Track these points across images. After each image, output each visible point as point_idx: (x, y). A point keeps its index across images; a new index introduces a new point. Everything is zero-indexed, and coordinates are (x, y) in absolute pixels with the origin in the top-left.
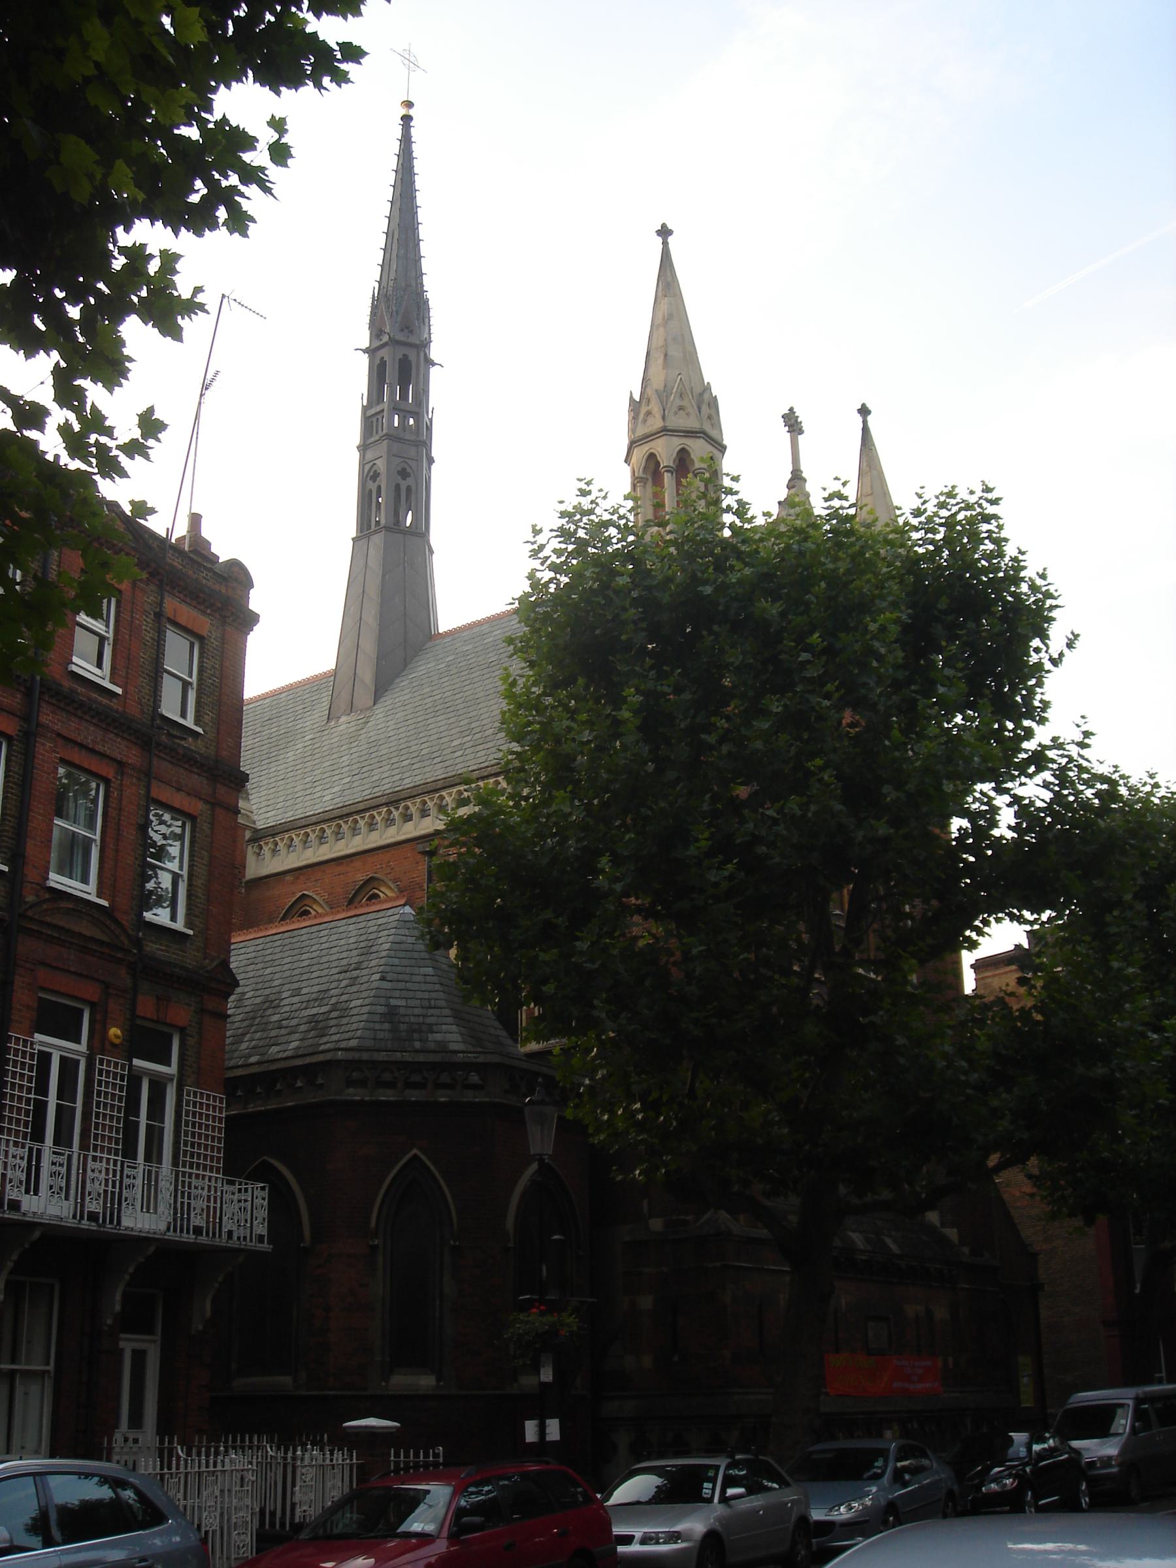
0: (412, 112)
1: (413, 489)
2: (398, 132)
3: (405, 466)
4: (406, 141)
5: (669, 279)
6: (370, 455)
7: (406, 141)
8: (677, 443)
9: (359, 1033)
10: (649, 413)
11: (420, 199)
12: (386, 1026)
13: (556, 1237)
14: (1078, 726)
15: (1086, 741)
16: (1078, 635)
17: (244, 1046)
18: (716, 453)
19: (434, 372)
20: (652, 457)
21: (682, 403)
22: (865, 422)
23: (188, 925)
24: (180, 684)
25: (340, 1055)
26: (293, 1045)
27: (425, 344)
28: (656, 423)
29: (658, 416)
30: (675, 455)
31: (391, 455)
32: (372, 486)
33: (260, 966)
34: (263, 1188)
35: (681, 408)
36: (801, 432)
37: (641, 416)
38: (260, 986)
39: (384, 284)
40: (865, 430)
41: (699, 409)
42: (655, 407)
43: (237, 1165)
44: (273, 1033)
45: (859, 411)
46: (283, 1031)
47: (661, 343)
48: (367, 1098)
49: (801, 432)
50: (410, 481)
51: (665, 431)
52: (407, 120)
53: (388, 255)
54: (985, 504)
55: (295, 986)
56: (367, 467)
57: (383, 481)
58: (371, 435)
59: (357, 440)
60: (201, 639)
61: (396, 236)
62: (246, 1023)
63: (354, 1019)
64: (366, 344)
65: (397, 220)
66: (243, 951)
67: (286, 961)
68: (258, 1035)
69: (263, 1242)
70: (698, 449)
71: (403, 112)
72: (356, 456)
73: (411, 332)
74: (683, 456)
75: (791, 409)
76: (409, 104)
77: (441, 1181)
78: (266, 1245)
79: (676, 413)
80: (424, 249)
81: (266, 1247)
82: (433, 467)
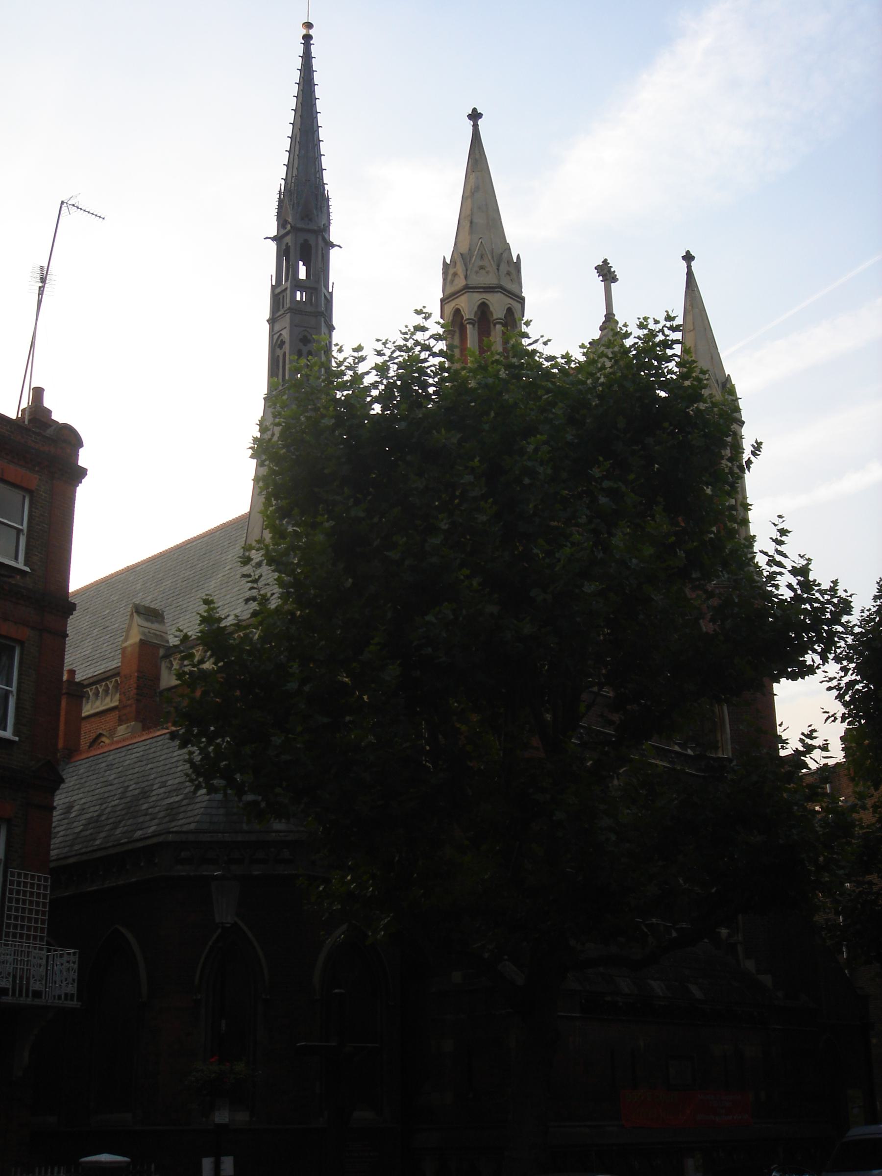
0: (311, 32)
2: (300, 49)
4: (307, 57)
5: (477, 156)
6: (277, 327)
7: (307, 57)
8: (477, 298)
9: (197, 818)
10: (455, 274)
11: (320, 106)
12: (222, 811)
13: (336, 991)
14: (775, 525)
15: (784, 538)
16: (761, 443)
17: (118, 831)
18: (516, 306)
19: (333, 253)
20: (457, 312)
21: (481, 263)
22: (689, 267)
23: (16, 732)
24: (14, 532)
25: (170, 837)
26: (153, 828)
27: (325, 229)
28: (460, 282)
29: (462, 277)
30: (476, 308)
31: (293, 325)
32: (279, 352)
33: (144, 763)
34: (74, 953)
35: (482, 268)
36: (614, 279)
37: (449, 277)
38: (140, 780)
39: (289, 181)
40: (690, 275)
41: (498, 266)
42: (460, 269)
43: (59, 933)
44: (141, 820)
45: (684, 258)
46: (148, 818)
47: (469, 212)
48: (192, 874)
49: (614, 279)
51: (467, 289)
52: (307, 38)
53: (292, 156)
54: (667, 332)
55: (164, 779)
56: (276, 337)
57: (287, 347)
58: (279, 310)
59: (267, 314)
60: (30, 492)
61: (298, 139)
62: (123, 812)
63: (198, 806)
64: (274, 232)
65: (299, 126)
66: (135, 750)
67: (163, 757)
68: (130, 822)
69: (72, 1000)
70: (498, 304)
71: (304, 32)
72: (267, 327)
73: (310, 220)
74: (483, 310)
75: (605, 262)
76: (308, 25)
77: (210, 943)
78: (75, 1002)
79: (477, 272)
80: (324, 148)
81: (75, 1003)
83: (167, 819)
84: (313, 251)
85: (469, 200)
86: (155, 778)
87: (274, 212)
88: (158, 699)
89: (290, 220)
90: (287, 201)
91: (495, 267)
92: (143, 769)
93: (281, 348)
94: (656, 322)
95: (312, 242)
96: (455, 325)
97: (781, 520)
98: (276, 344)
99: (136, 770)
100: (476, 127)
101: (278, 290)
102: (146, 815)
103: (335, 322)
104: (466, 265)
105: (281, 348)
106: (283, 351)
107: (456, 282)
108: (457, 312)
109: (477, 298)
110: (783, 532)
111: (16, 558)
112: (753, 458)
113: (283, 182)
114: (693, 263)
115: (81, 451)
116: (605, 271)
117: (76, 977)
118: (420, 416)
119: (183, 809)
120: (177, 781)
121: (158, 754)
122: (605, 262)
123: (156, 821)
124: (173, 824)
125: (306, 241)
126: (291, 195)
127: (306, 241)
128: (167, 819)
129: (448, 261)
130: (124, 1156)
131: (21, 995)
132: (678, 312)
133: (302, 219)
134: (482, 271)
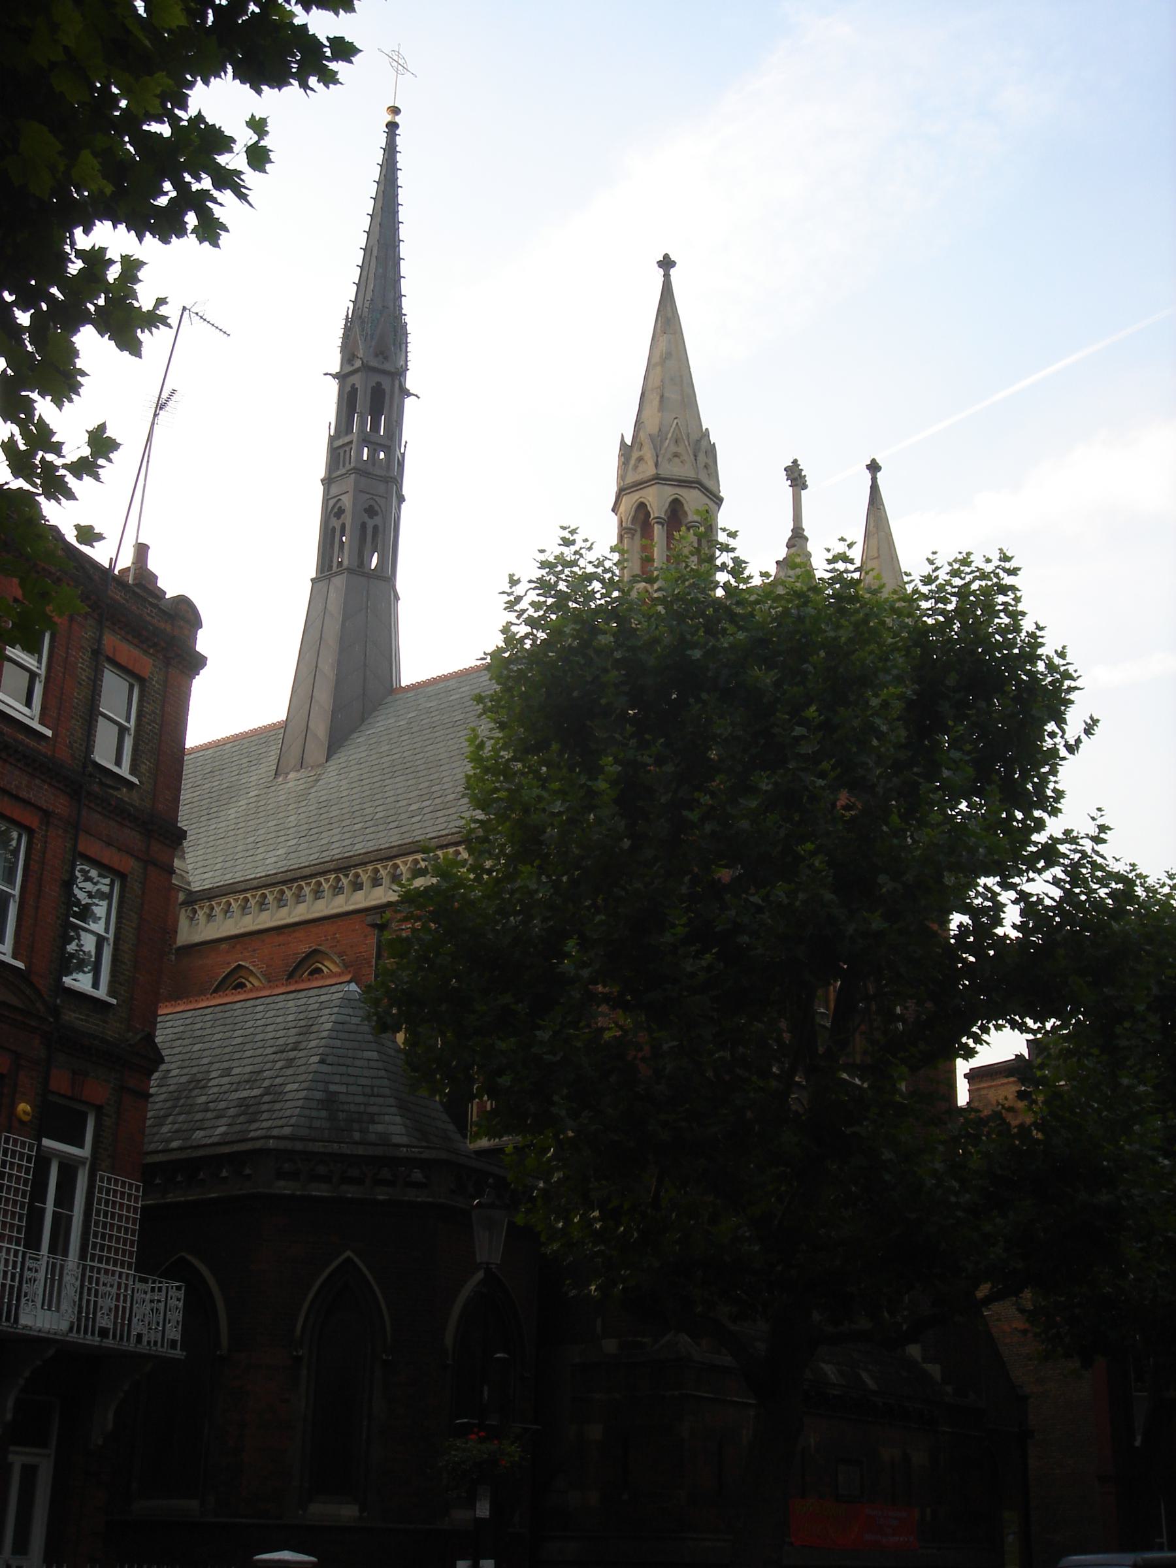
0: (398, 119)
1: (381, 529)
3: (372, 503)
4: (390, 150)
5: (670, 315)
6: (334, 490)
7: (390, 150)
8: (669, 492)
9: (293, 1121)
12: (324, 1114)
14: (1093, 819)
16: (1098, 721)
17: (165, 1129)
19: (409, 402)
20: (642, 506)
23: (112, 992)
24: (116, 728)
25: (271, 1143)
26: (222, 1129)
27: (401, 372)
28: (648, 470)
29: (651, 463)
31: (358, 491)
32: (337, 524)
34: (178, 1288)
35: (676, 455)
36: (805, 487)
37: (632, 462)
38: (186, 1063)
39: (359, 304)
40: (874, 488)
42: (648, 453)
43: (153, 1260)
44: (199, 1116)
45: (868, 467)
46: (209, 1115)
48: (298, 1193)
49: (805, 487)
50: (377, 520)
51: (658, 479)
52: (392, 127)
53: (365, 273)
54: (1002, 574)
55: (226, 1065)
56: (332, 502)
57: (348, 518)
59: (322, 473)
60: (141, 680)
61: (375, 253)
62: (168, 1104)
64: (336, 368)
68: (182, 1118)
70: (692, 500)
71: (389, 118)
73: (386, 358)
74: (676, 510)
75: (795, 462)
76: (395, 110)
78: (178, 1351)
79: (670, 460)
82: (404, 506)
83: (242, 1119)
84: (387, 397)
85: (659, 369)
86: (211, 1063)
87: (339, 342)
88: (173, 958)
89: (360, 355)
90: (357, 329)
91: (692, 457)
92: (188, 1049)
93: (339, 518)
94: (988, 561)
95: (386, 385)
96: (637, 525)
97: (1100, 813)
98: (332, 513)
99: (248, 1054)
100: (667, 276)
101: (340, 442)
102: (207, 1111)
103: (406, 491)
104: (655, 448)
105: (339, 518)
106: (340, 522)
107: (640, 469)
108: (642, 506)
109: (669, 492)
110: (1103, 828)
111: (118, 763)
112: (1084, 737)
113: (351, 305)
114: (879, 475)
115: (200, 632)
116: (796, 475)
117: (180, 1319)
118: (726, 645)
119: (265, 1107)
120: (248, 1069)
121: (208, 1031)
122: (795, 462)
123: (224, 1121)
124: (254, 1126)
125: (379, 384)
126: (363, 322)
127: (379, 384)
128: (242, 1119)
129: (629, 442)
130: (265, 1561)
131: (121, 1338)
132: (857, 533)
133: (377, 356)
134: (676, 459)
